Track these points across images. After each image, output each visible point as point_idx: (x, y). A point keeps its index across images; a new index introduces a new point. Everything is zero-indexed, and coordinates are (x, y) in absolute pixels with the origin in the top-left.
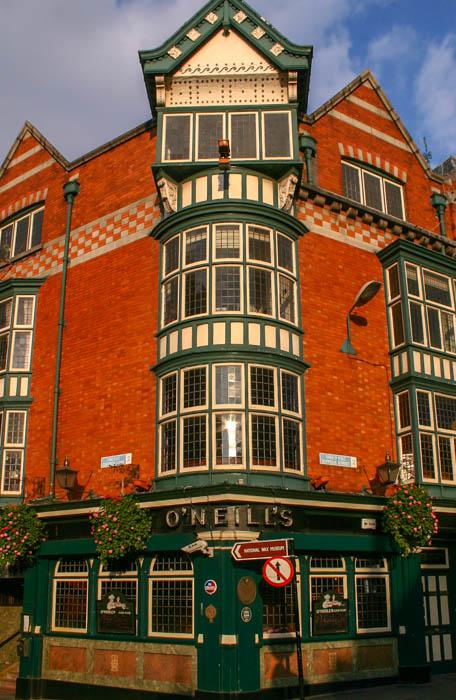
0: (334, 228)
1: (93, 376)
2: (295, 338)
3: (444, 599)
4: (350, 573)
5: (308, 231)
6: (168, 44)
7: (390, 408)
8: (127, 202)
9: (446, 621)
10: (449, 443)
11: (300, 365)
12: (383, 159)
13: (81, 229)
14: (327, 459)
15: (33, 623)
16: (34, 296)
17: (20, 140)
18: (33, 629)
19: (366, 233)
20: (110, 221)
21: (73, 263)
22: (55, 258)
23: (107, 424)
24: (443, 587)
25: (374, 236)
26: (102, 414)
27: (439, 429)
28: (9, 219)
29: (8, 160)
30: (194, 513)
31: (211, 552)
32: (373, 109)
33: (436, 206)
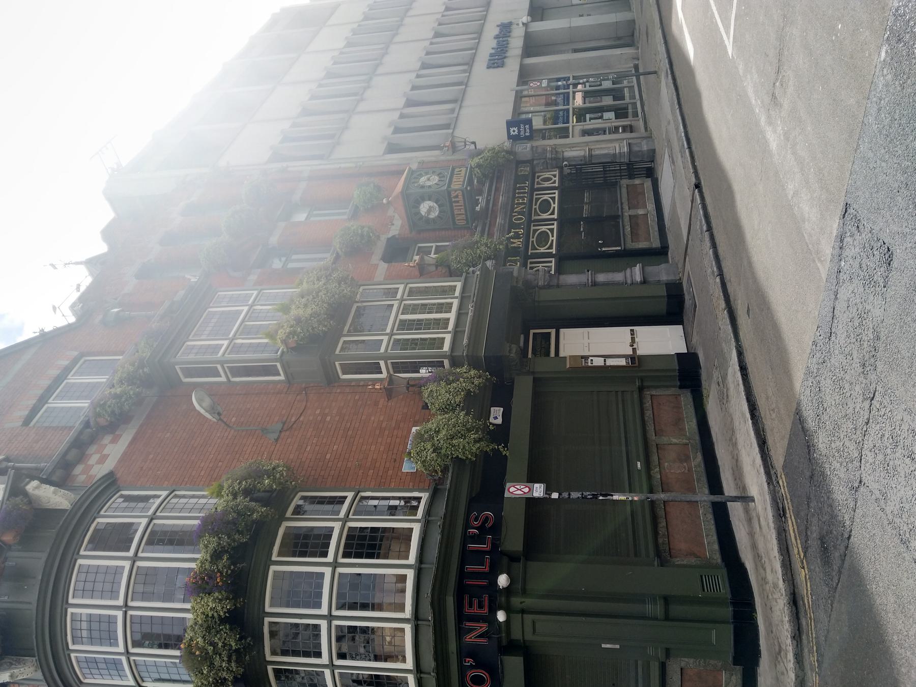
5: (111, 474)
10: (406, 321)
27: (388, 331)
30: (470, 638)
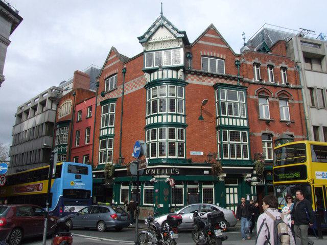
0: (198, 80)
2: (183, 118)
3: (236, 196)
4: (185, 187)
6: (145, 34)
7: (216, 136)
8: (138, 76)
11: (184, 126)
12: (217, 53)
13: (127, 83)
14: (192, 153)
15: (115, 202)
17: (111, 52)
19: (209, 80)
20: (134, 82)
21: (125, 94)
25: (212, 80)
28: (108, 78)
29: (107, 58)
31: (157, 181)
32: (214, 36)
33: (237, 65)
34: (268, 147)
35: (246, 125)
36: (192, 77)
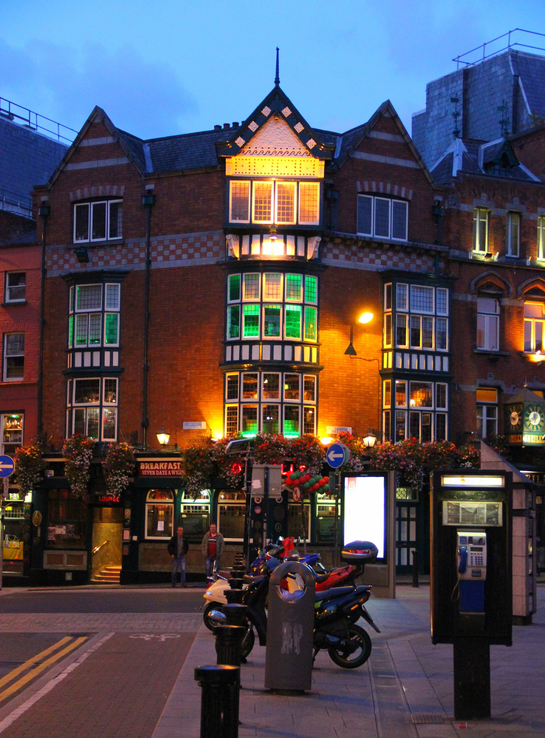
0: (348, 258)
1: (175, 362)
3: (413, 524)
9: (413, 538)
12: (393, 184)
15: (132, 535)
16: (119, 284)
18: (132, 538)
19: (372, 256)
21: (154, 266)
22: (136, 256)
23: (187, 399)
24: (413, 516)
26: (183, 391)
34: (488, 415)
35: (446, 368)
36: (336, 251)
